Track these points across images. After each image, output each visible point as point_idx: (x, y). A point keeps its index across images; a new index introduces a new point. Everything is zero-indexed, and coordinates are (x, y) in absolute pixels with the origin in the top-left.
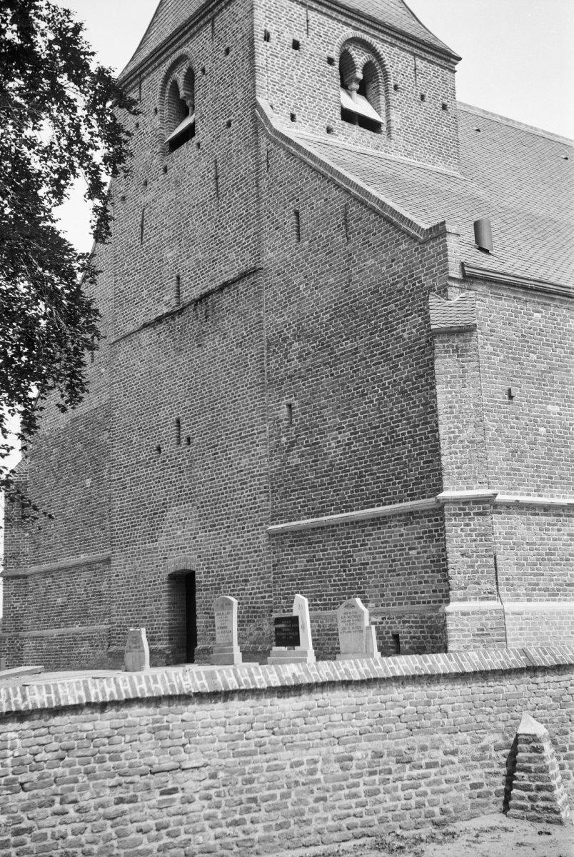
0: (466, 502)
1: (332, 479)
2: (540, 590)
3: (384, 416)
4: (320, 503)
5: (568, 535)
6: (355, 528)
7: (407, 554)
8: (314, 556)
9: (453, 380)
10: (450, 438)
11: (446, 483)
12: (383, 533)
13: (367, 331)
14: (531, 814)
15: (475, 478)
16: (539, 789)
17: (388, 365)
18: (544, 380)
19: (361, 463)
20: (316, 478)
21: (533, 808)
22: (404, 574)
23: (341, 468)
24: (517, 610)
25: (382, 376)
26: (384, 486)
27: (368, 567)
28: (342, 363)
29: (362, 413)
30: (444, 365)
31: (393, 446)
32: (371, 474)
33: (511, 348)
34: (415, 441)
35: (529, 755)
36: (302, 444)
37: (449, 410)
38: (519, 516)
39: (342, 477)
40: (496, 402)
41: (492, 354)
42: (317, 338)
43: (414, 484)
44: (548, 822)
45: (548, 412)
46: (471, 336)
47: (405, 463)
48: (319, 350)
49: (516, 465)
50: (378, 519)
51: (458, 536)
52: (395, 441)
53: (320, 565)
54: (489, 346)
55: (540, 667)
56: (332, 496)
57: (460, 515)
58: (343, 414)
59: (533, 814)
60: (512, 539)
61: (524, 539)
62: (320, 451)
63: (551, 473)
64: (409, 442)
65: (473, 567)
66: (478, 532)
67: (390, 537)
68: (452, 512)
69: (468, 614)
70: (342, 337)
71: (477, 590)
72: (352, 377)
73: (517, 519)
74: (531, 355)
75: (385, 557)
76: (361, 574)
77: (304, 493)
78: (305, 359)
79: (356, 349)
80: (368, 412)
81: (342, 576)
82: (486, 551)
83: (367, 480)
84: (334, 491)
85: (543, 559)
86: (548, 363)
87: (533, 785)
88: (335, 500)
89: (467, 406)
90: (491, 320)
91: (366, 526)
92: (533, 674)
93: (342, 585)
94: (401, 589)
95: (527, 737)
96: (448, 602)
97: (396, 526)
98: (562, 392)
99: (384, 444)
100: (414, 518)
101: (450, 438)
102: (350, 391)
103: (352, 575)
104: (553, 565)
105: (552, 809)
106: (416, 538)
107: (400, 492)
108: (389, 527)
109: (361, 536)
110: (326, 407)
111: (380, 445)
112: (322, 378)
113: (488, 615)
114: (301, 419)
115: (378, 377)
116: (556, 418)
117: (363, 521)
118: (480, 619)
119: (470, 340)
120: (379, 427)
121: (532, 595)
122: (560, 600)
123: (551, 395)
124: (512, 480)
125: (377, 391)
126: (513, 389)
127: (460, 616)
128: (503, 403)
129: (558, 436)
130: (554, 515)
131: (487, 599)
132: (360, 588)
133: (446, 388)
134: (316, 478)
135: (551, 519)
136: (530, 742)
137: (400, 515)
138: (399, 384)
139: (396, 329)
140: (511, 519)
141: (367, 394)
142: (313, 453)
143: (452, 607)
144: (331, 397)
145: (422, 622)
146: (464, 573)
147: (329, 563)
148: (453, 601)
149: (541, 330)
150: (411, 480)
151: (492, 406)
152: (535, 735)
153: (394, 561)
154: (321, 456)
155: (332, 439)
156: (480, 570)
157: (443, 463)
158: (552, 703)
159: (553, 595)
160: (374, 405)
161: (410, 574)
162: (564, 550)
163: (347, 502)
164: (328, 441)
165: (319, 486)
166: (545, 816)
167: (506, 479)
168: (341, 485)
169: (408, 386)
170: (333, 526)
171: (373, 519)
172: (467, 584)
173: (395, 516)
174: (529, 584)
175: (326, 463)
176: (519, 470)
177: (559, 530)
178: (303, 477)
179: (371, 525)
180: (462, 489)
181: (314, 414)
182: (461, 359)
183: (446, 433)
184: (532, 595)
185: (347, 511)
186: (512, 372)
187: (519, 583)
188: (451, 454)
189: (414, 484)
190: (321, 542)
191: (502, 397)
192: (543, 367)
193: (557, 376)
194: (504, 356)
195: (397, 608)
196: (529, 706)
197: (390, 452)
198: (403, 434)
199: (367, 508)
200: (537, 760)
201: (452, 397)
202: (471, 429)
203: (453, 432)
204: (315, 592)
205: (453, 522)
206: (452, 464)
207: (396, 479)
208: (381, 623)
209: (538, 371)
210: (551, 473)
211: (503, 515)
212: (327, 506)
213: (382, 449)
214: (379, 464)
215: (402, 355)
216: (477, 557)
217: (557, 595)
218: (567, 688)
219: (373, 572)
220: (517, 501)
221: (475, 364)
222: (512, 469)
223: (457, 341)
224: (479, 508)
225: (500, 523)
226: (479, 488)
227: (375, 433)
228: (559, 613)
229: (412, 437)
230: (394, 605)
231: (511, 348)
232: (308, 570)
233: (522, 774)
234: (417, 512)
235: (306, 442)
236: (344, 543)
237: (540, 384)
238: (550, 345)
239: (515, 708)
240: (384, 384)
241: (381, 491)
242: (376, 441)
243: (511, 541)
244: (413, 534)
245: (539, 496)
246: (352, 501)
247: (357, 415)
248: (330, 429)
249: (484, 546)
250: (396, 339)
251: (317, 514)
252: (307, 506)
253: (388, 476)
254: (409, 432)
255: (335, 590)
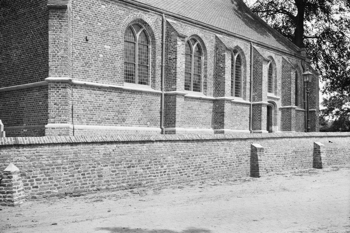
0: (58, 82)
1: (13, 70)
2: (93, 121)
3: (34, 44)
4: (9, 81)
5: (109, 99)
6: (21, 92)
7: (38, 104)
8: (5, 103)
9: (56, 29)
10: (53, 54)
11: (50, 74)
12: (30, 94)
13: (29, 5)
14: (3, 203)
15: (63, 72)
16: (8, 193)
17: (36, 21)
18: (104, 35)
19: (24, 64)
20: (8, 70)
21: (4, 201)
22: (37, 112)
23: (17, 66)
24: (80, 128)
25: (34, 26)
26: (32, 74)
27: (24, 108)
28: (19, 19)
29: (26, 42)
30: (53, 22)
31: (36, 57)
32: (28, 69)
33: (89, 19)
34: (44, 55)
35: (6, 179)
36: (3, 54)
37: (53, 42)
38: (86, 90)
39: (17, 70)
40: (79, 41)
41: (79, 20)
42: (10, 6)
43: (43, 74)
44: (9, 206)
45: (105, 48)
46: (65, 11)
47: (40, 65)
48: (11, 12)
49: (87, 69)
50: (29, 88)
51: (53, 96)
52: (37, 55)
53: (7, 107)
54: (78, 17)
55: (20, 145)
56: (13, 78)
57: (55, 87)
58: (19, 42)
59: (4, 203)
60: (82, 99)
61: (88, 100)
62: (10, 58)
63: (103, 73)
64: (42, 56)
65: (59, 109)
66: (62, 95)
67: (33, 96)
68: (52, 86)
69: (55, 128)
70: (19, 7)
71: (60, 119)
72: (23, 25)
73: (85, 91)
74: (98, 23)
75: (30, 105)
76: (22, 111)
77: (3, 76)
78: (5, 16)
79: (25, 13)
80: (28, 42)
81: (15, 112)
82: (65, 103)
83: (26, 72)
84: (14, 76)
85: (96, 108)
86: (106, 28)
87: (6, 191)
88: (14, 79)
89: (61, 41)
90: (80, 6)
91: (24, 91)
92: (17, 147)
93: (15, 116)
94: (36, 118)
95: (7, 173)
96: (47, 124)
97: (35, 92)
98: (112, 40)
99: (33, 56)
100: (42, 88)
101: (53, 54)
102: (22, 32)
103: (19, 112)
104: (100, 111)
105: (11, 200)
106: (42, 97)
107: (38, 77)
108: (33, 92)
109: (22, 95)
110: (13, 38)
111: (31, 57)
112: (12, 25)
113: (63, 129)
114: (3, 43)
115: (32, 26)
116: (108, 51)
117: (24, 89)
118: (60, 131)
119: (65, 13)
120: (31, 48)
121: (89, 123)
122: (102, 125)
123: (107, 41)
124: (84, 75)
125: (31, 33)
126: (88, 37)
127: (51, 129)
128: (83, 42)
129: (108, 59)
130: (103, 91)
131: (64, 123)
132: (21, 117)
133: (53, 32)
134: (8, 70)
135: (101, 92)
136: (8, 174)
137: (37, 87)
138: (40, 30)
139: (40, 5)
140: (82, 91)
141: (28, 34)
142: (7, 59)
143: (48, 125)
144: (15, 34)
145: (41, 132)
146: (55, 112)
147: (11, 107)
148: (49, 123)
149: (104, 13)
150: (42, 72)
151: (77, 43)
152: (10, 172)
153: (34, 106)
154: (10, 60)
155: (15, 53)
156: (62, 111)
157: (49, 65)
158: (26, 159)
159: (99, 123)
160: (30, 39)
161: (39, 112)
162: (106, 105)
163: (18, 81)
164: (13, 53)
165: (9, 73)
166: (8, 203)
167: (81, 74)
168: (17, 73)
169: (43, 31)
170: (13, 91)
171: (27, 89)
172: (55, 116)
173: (35, 87)
174: (88, 118)
175: (11, 63)
176: (88, 71)
177: (105, 97)
178: (3, 69)
179: (26, 91)
180: (56, 77)
181: (8, 41)
182: (60, 21)
183: (51, 52)
184: (89, 123)
185: (18, 85)
186: (89, 29)
187: (84, 117)
188: (53, 61)
189: (43, 74)
190: (8, 97)
191: (82, 40)
192: (104, 29)
193: (111, 33)
194: (85, 22)
195: (33, 126)
196: (14, 160)
197: (35, 60)
198: (40, 52)
199: (26, 83)
200: (9, 181)
201: (55, 37)
202: (62, 51)
203: (55, 52)
204: (5, 118)
205: (52, 90)
206: (53, 65)
207: (37, 71)
208: (27, 132)
209: (101, 30)
210: (103, 73)
211: (78, 89)
212: (11, 82)
213: (32, 58)
214: (31, 65)
215: (41, 17)
216: (61, 105)
217: (101, 123)
218: (34, 153)
219: (26, 111)
220: (85, 84)
221: (66, 23)
222: (85, 71)
223: (59, 13)
224: (63, 85)
225: (76, 92)
226: (64, 76)
227: (30, 51)
228: (100, 130)
229: (43, 54)
230: (33, 125)
231: (89, 19)
232: (3, 109)
233: (2, 187)
234: (43, 86)
235: (5, 53)
236: (16, 98)
237: (102, 36)
238: (108, 20)
239: (6, 161)
240: (34, 30)
241: (31, 76)
242: (30, 55)
243: (81, 100)
244: (41, 95)
245: (97, 82)
246: (20, 80)
247: (24, 43)
248: (14, 48)
249: (64, 101)
250: (39, 10)
251: (7, 85)
252: (4, 81)
253: (34, 70)
254: (42, 52)
255: (12, 118)
